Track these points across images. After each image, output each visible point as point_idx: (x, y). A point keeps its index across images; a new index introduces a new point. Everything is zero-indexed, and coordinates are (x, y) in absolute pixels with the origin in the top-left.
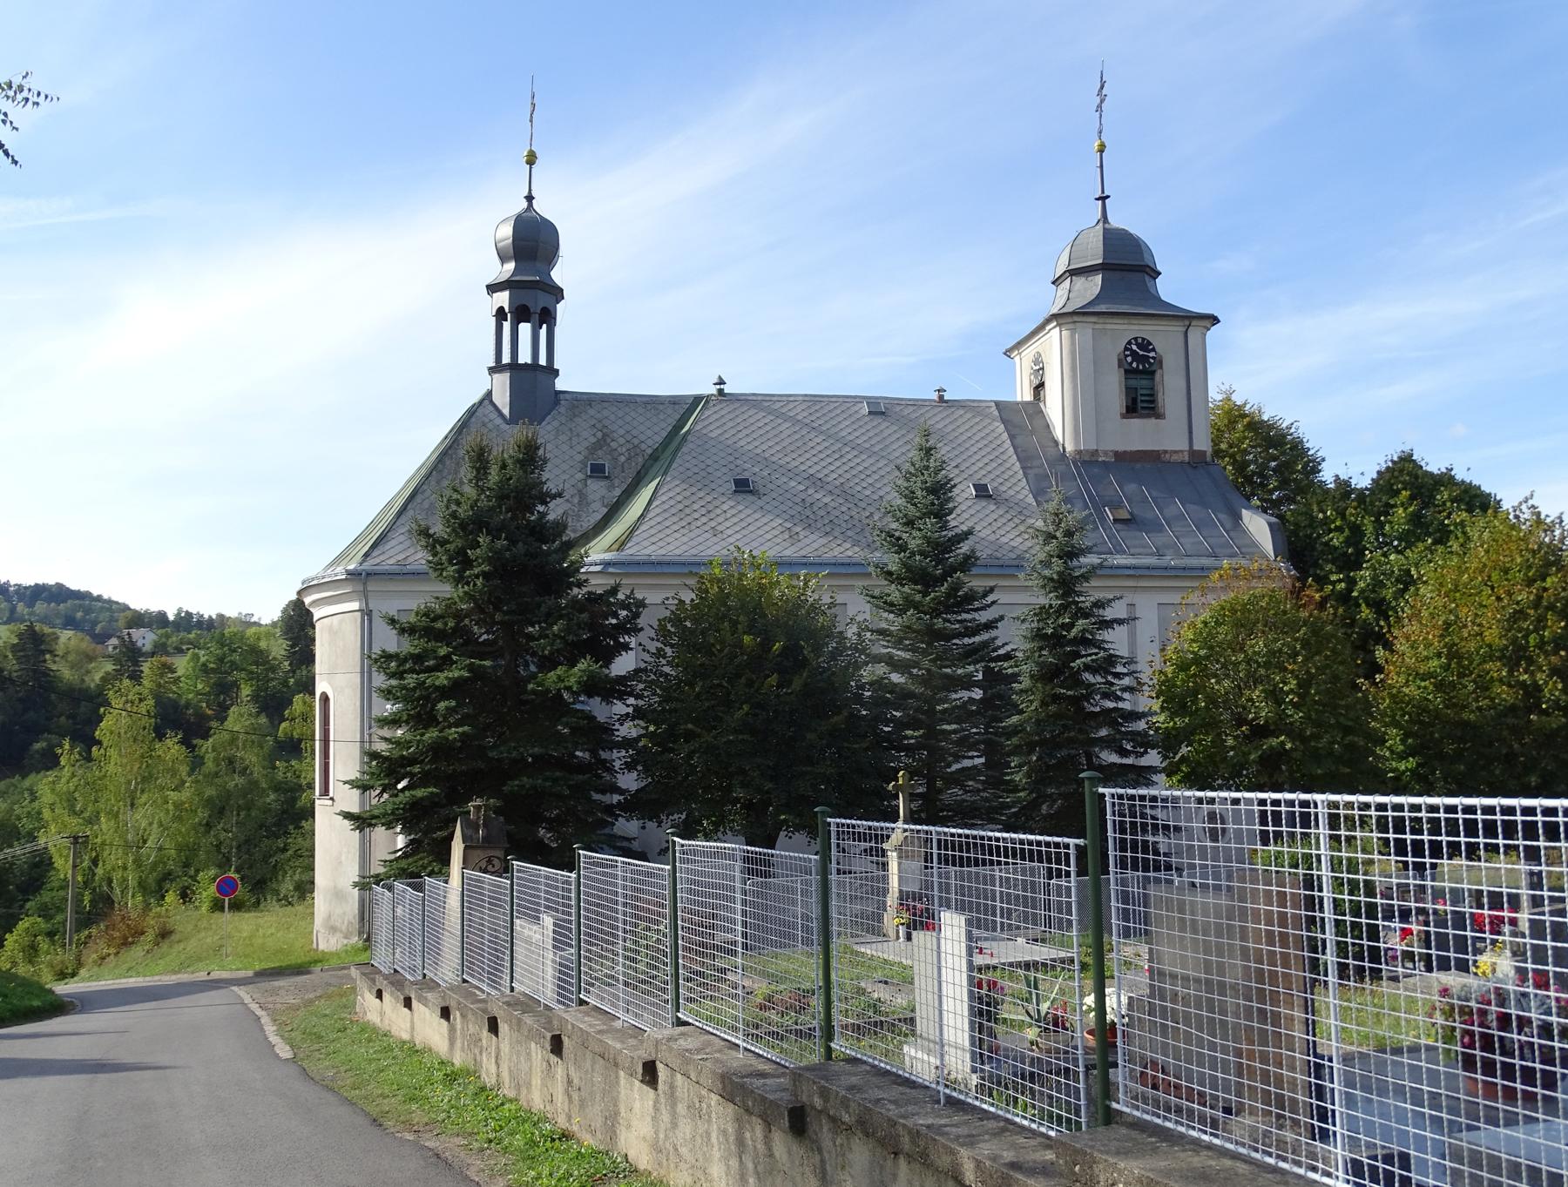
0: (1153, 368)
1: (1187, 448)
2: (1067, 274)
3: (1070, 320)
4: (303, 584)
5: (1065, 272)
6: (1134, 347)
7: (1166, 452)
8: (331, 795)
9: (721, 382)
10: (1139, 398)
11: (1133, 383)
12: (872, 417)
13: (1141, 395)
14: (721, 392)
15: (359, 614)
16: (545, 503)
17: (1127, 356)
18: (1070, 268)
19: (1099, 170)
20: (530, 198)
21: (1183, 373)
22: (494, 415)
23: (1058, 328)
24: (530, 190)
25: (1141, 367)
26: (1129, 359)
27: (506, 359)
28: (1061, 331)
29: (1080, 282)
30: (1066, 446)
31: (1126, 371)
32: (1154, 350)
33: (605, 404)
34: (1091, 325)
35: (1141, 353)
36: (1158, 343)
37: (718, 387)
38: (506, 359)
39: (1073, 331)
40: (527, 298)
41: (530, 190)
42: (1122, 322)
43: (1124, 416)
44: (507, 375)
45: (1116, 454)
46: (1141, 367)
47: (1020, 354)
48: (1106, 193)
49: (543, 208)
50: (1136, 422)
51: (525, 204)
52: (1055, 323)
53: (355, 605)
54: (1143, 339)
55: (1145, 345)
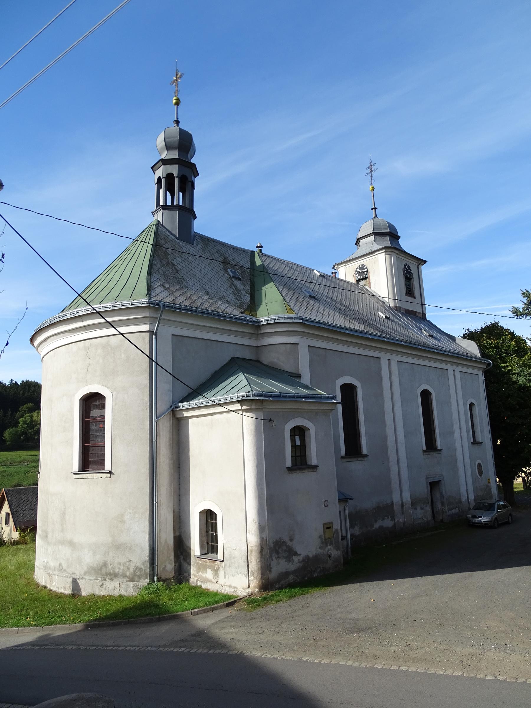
2: (160, 163)
3: (391, 250)
4: (369, 272)
5: (372, 233)
6: (358, 270)
8: (108, 466)
15: (148, 334)
17: (405, 270)
18: (374, 232)
23: (384, 253)
26: (357, 275)
27: (169, 203)
28: (385, 255)
30: (390, 303)
34: (396, 254)
38: (161, 203)
39: (391, 256)
44: (176, 213)
47: (345, 266)
48: (376, 207)
52: (384, 251)
53: (147, 327)
54: (362, 265)
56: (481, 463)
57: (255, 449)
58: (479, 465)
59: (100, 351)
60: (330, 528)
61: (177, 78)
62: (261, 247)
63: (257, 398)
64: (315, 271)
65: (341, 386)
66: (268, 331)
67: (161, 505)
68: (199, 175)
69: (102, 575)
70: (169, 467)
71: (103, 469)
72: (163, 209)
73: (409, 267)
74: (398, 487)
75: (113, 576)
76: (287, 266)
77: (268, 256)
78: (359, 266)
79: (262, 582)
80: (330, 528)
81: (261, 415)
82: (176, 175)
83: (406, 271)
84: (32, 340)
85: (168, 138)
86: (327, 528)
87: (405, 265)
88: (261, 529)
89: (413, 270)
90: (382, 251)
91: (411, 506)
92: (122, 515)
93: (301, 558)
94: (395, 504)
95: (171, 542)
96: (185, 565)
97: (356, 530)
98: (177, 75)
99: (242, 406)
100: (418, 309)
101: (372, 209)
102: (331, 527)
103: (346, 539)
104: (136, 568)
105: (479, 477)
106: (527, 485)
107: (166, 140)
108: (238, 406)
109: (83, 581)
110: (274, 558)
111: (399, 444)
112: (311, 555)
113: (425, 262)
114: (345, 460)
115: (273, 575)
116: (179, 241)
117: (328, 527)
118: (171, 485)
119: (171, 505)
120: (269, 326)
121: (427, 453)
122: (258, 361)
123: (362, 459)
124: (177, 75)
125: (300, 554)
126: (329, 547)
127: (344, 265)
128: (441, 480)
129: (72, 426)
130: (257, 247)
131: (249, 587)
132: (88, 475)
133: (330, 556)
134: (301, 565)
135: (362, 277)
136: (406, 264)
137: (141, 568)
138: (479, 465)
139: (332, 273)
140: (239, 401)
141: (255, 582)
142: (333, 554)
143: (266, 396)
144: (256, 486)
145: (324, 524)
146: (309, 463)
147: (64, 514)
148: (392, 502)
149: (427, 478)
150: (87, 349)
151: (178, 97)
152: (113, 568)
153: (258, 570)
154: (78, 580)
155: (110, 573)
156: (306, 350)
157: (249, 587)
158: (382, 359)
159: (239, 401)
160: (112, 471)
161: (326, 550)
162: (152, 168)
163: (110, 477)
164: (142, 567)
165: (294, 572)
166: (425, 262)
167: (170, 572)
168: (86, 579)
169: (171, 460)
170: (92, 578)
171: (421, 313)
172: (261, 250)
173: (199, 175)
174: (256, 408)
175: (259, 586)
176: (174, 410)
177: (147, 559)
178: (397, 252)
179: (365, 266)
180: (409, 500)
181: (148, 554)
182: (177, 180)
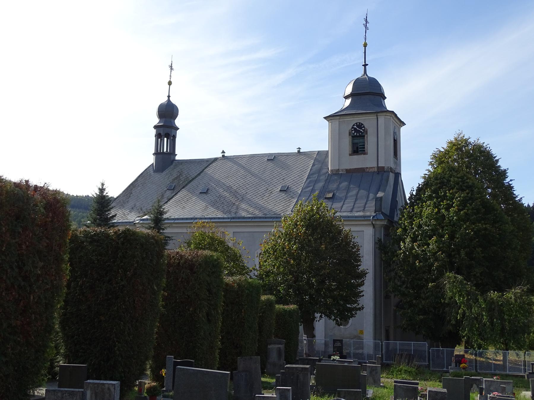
0: (363, 134)
1: (376, 166)
6: (355, 127)
7: (367, 168)
9: (223, 152)
10: (359, 147)
11: (356, 141)
12: (268, 161)
13: (360, 146)
14: (223, 156)
17: (353, 130)
19: (364, 53)
20: (169, 97)
24: (169, 94)
25: (358, 135)
26: (353, 132)
31: (352, 137)
32: (364, 127)
33: (186, 163)
34: (338, 120)
35: (358, 129)
36: (366, 125)
37: (223, 154)
40: (167, 130)
41: (169, 94)
42: (352, 117)
43: (350, 155)
45: (347, 170)
46: (358, 135)
49: (173, 100)
50: (355, 157)
51: (167, 98)
55: (360, 125)
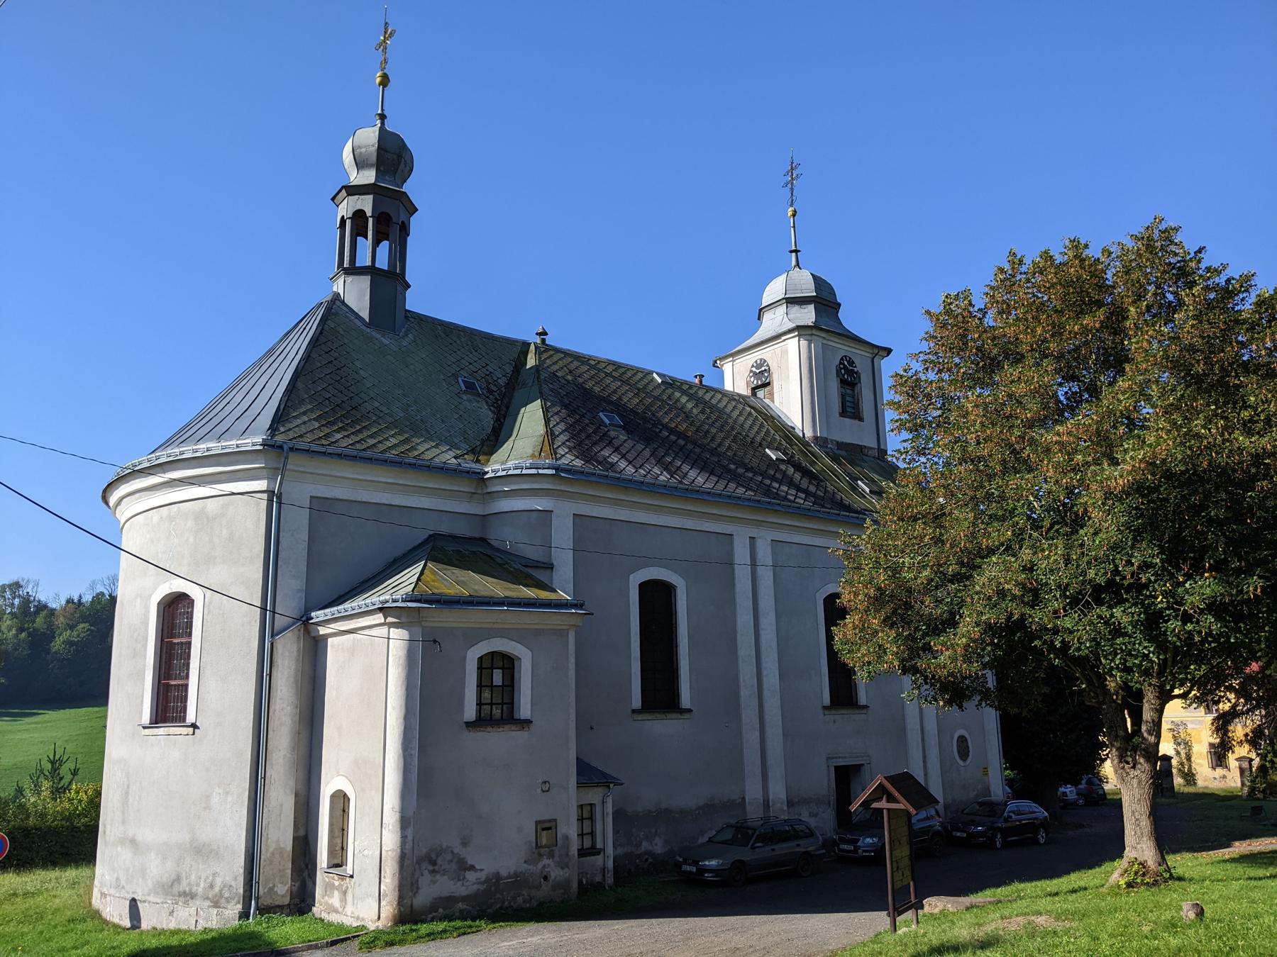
5: (783, 299)
6: (754, 369)
8: (191, 717)
16: (839, 598)
17: (841, 369)
18: (787, 296)
21: (872, 389)
22: (359, 324)
26: (752, 379)
28: (799, 341)
29: (795, 309)
34: (821, 339)
39: (810, 342)
47: (733, 361)
52: (796, 333)
53: (262, 485)
54: (761, 360)
56: (967, 736)
57: (404, 688)
58: (962, 740)
59: (190, 523)
60: (549, 829)
61: (385, 37)
62: (545, 333)
63: (410, 604)
64: (655, 375)
65: (640, 585)
66: (498, 488)
67: (273, 781)
68: (417, 210)
69: (174, 896)
70: (292, 720)
71: (184, 720)
72: (345, 274)
73: (851, 363)
74: (758, 770)
75: (189, 896)
76: (583, 363)
77: (557, 350)
78: (756, 362)
79: (399, 910)
80: (549, 829)
81: (418, 632)
82: (369, 213)
83: (843, 371)
84: (105, 500)
85: (359, 147)
86: (544, 829)
87: (842, 359)
88: (405, 822)
89: (861, 366)
90: (793, 335)
91: (785, 808)
92: (208, 797)
93: (483, 876)
94: (749, 803)
95: (288, 844)
96: (309, 884)
97: (656, 845)
98: (385, 32)
99: (385, 619)
100: (870, 442)
101: (792, 252)
102: (553, 828)
103: (602, 853)
104: (224, 887)
105: (961, 763)
106: (1, 663)
107: (357, 151)
108: (379, 618)
109: (146, 904)
110: (426, 873)
111: (766, 694)
112: (504, 873)
113: (889, 351)
114: (641, 717)
115: (422, 899)
116: (368, 330)
117: (546, 826)
118: (293, 749)
119: (292, 783)
120: (497, 481)
121: (834, 712)
122: (483, 541)
123: (678, 716)
124: (385, 32)
125: (482, 870)
126: (546, 861)
127: (731, 359)
128: (863, 765)
129: (145, 646)
130: (539, 334)
131: (379, 918)
132: (162, 729)
133: (545, 878)
134: (482, 887)
135: (760, 383)
136: (846, 356)
137: (231, 886)
138: (962, 740)
139: (696, 377)
140: (381, 609)
141: (389, 909)
142: (553, 875)
143: (426, 602)
144: (401, 751)
145: (537, 823)
146: (516, 716)
147: (127, 793)
148: (744, 799)
149: (828, 758)
150: (199, 516)
151: (385, 71)
152: (189, 884)
153: (394, 890)
154: (138, 902)
155: (185, 892)
156: (569, 522)
157: (379, 918)
158: (735, 537)
159: (381, 609)
160: (198, 724)
161: (540, 865)
162: (333, 199)
163: (194, 734)
164: (233, 884)
165: (465, 899)
166: (889, 351)
167: (283, 896)
168: (149, 902)
169: (297, 707)
170: (159, 901)
171: (874, 449)
172: (543, 340)
173: (417, 210)
174: (409, 620)
175: (394, 916)
176: (304, 621)
177: (242, 871)
178: (824, 335)
179: (765, 361)
180: (784, 797)
181: (243, 864)
182: (371, 220)
